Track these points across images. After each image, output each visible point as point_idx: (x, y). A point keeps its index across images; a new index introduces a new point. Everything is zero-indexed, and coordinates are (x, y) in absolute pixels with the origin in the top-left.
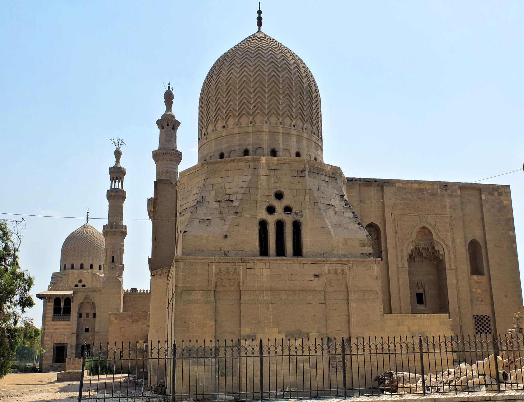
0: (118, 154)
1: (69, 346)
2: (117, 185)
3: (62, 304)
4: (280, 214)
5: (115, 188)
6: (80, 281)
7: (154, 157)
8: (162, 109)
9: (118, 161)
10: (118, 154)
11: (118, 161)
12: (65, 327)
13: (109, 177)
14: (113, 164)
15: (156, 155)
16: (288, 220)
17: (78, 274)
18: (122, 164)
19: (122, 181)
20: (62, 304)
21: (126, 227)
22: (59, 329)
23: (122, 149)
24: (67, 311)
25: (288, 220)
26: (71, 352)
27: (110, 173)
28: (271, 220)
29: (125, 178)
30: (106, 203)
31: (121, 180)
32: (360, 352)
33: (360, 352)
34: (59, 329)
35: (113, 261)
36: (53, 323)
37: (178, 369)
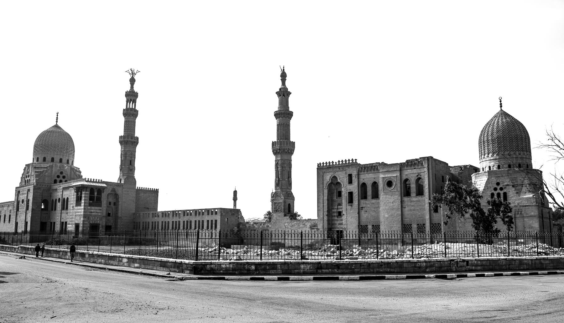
0: (132, 81)
1: (100, 226)
2: (131, 106)
3: (96, 193)
4: (498, 191)
5: (129, 108)
6: (62, 173)
7: (275, 115)
8: (279, 85)
9: (132, 87)
10: (132, 81)
11: (132, 87)
12: (98, 211)
13: (125, 99)
14: (128, 89)
15: (277, 115)
16: (502, 192)
17: (60, 167)
18: (136, 89)
19: (135, 103)
20: (96, 193)
21: (138, 138)
22: (94, 212)
23: (135, 77)
24: (99, 200)
25: (502, 192)
26: (102, 229)
27: (126, 96)
28: (495, 193)
29: (138, 100)
30: (122, 119)
31: (134, 102)
32: (310, 238)
33: (310, 238)
34: (94, 212)
35: (131, 164)
36: (89, 208)
37: (479, 247)
